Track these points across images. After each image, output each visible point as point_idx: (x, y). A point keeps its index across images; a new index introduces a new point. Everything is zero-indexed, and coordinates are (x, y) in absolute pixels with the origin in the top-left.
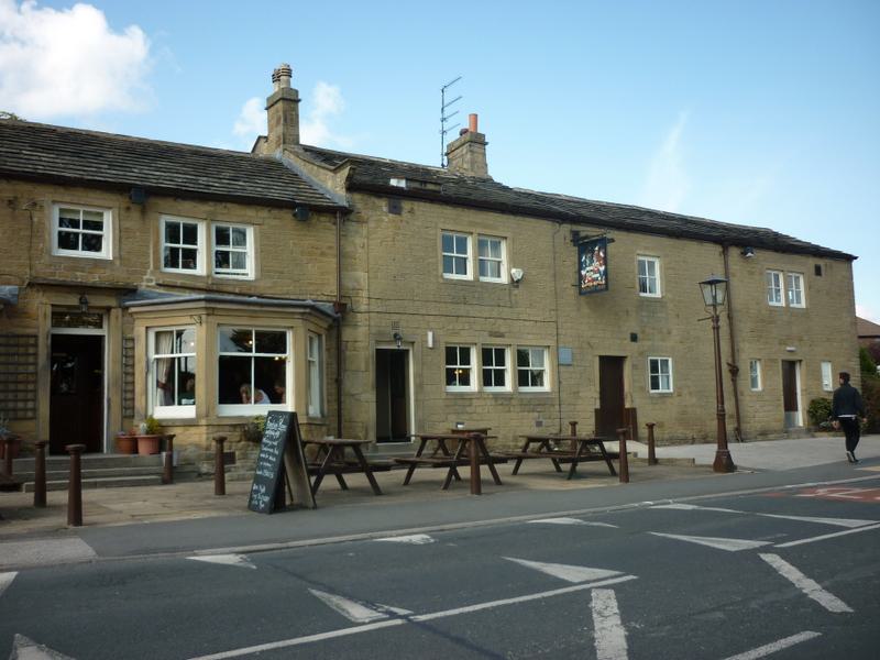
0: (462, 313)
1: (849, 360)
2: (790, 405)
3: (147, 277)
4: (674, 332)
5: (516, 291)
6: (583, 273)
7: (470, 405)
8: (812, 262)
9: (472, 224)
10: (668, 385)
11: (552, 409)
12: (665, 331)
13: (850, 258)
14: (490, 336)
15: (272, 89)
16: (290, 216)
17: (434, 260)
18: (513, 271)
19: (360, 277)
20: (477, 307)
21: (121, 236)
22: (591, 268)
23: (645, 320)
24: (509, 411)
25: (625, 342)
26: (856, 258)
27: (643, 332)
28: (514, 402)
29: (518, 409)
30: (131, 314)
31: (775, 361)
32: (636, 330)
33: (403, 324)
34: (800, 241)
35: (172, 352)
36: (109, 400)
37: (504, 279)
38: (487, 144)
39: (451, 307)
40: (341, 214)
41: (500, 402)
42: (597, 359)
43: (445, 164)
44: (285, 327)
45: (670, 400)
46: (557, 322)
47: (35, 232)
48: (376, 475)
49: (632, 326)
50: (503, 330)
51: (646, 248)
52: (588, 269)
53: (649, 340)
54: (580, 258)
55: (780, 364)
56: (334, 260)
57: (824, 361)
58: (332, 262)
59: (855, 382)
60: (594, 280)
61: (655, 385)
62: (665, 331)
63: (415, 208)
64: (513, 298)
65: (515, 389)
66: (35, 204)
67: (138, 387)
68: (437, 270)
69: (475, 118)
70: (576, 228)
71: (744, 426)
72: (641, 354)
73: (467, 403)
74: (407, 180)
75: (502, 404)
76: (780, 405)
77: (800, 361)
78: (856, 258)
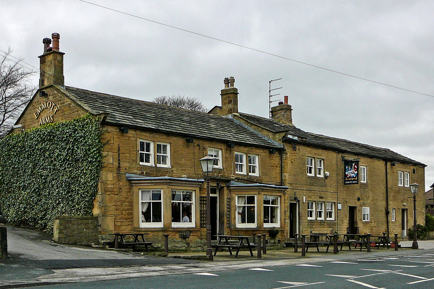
0: (312, 189)
1: (422, 209)
2: (403, 228)
3: (232, 175)
4: (370, 197)
5: (326, 181)
6: (347, 173)
8: (412, 167)
11: (335, 227)
12: (368, 196)
13: (424, 166)
14: (320, 198)
15: (223, 87)
16: (267, 152)
18: (326, 172)
21: (262, 165)
22: (351, 172)
23: (362, 192)
26: (426, 166)
27: (361, 197)
30: (132, 183)
32: (359, 196)
33: (297, 193)
34: (402, 156)
35: (245, 204)
37: (322, 176)
40: (281, 151)
43: (271, 116)
44: (192, 190)
46: (337, 193)
49: (358, 194)
50: (323, 196)
54: (345, 167)
55: (401, 210)
57: (340, 210)
58: (278, 170)
61: (364, 219)
62: (368, 196)
63: (300, 148)
65: (325, 219)
66: (204, 148)
67: (233, 217)
68: (306, 172)
69: (286, 98)
70: (343, 155)
74: (298, 137)
76: (53, 286)
77: (407, 209)
78: (426, 166)
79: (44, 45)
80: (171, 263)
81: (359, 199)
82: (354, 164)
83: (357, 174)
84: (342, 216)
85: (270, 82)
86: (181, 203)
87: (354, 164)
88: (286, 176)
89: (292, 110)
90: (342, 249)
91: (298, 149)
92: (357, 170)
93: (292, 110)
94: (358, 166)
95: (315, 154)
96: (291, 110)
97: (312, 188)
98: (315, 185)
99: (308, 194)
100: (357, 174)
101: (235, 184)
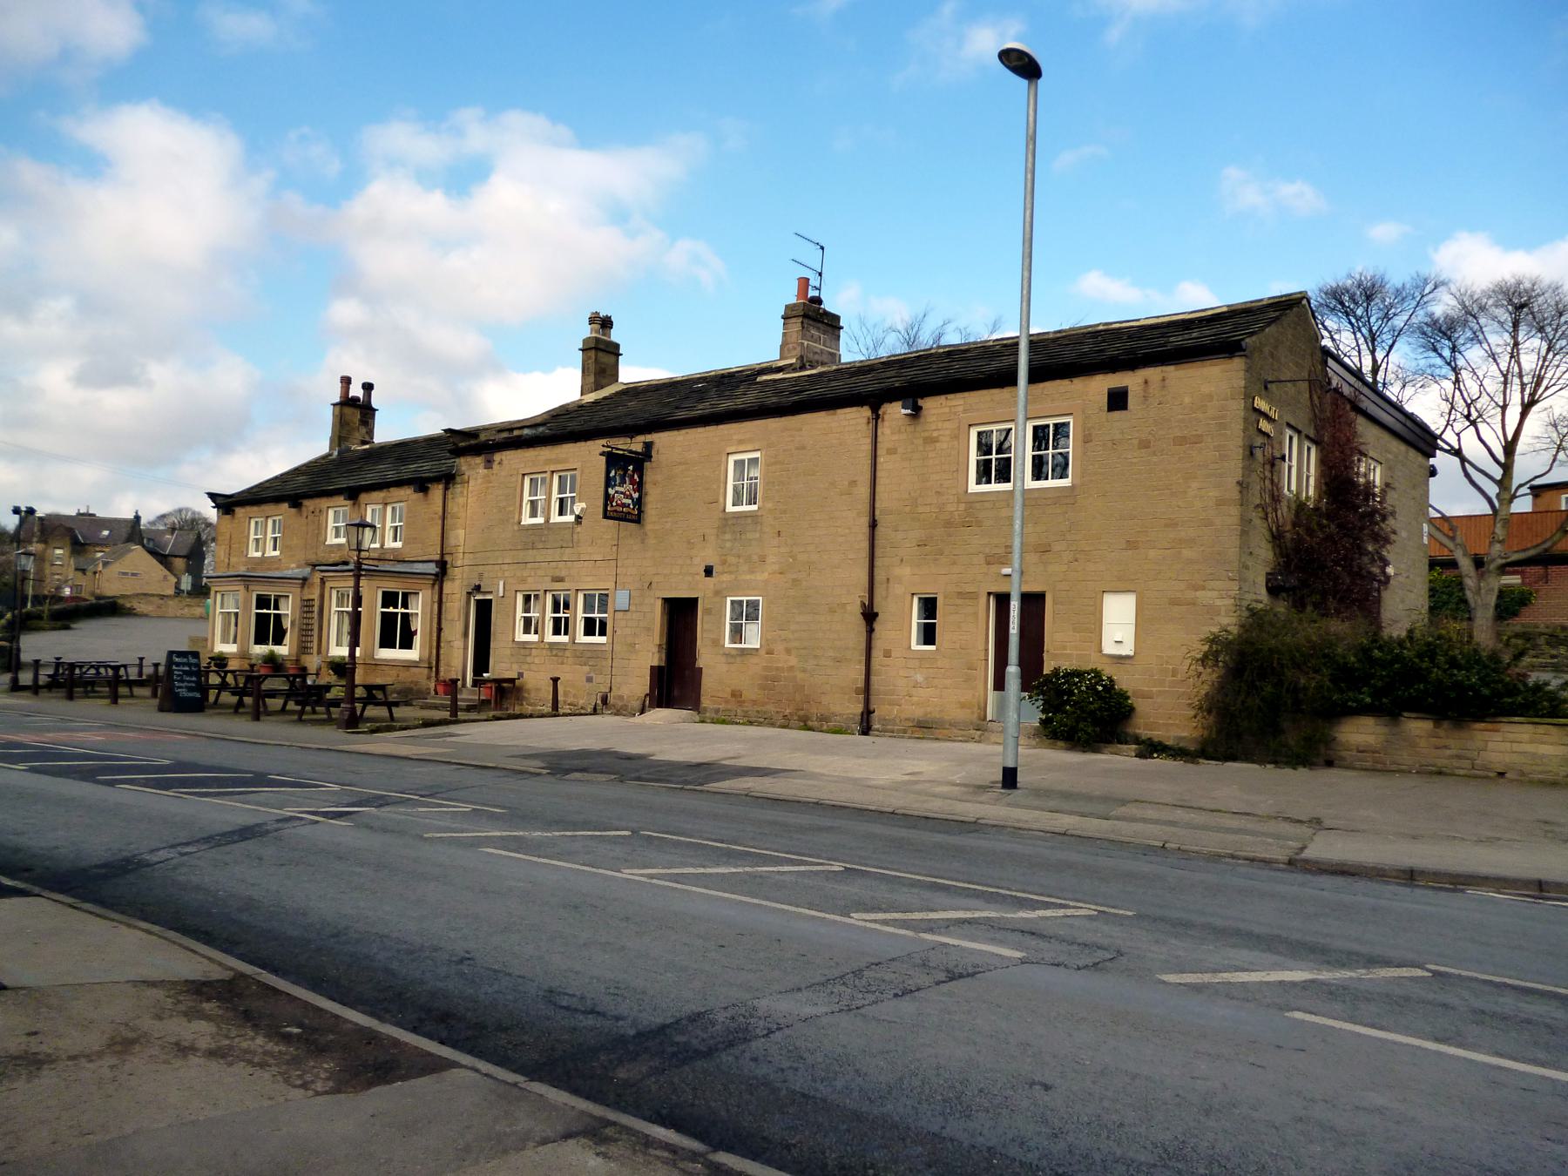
4: (771, 559)
5: (579, 529)
6: (611, 491)
7: (530, 655)
9: (549, 461)
10: (753, 636)
17: (511, 509)
19: (459, 536)
20: (544, 552)
23: (728, 545)
24: (562, 663)
25: (698, 577)
27: (724, 563)
28: (568, 654)
29: (570, 660)
31: (973, 596)
33: (486, 575)
36: (466, 634)
38: (842, 328)
39: (521, 553)
41: (554, 652)
42: (659, 603)
45: (754, 660)
47: (320, 530)
48: (394, 710)
50: (563, 574)
51: (741, 442)
52: (617, 488)
53: (731, 573)
54: (608, 472)
56: (1558, 457)
59: (161, 669)
60: (624, 505)
63: (504, 458)
64: (575, 536)
71: (881, 710)
72: (717, 593)
73: (527, 652)
75: (556, 656)
79: (340, 384)
80: (824, 855)
81: (709, 572)
82: (631, 468)
83: (640, 499)
84: (628, 631)
85: (822, 248)
86: (233, 615)
87: (631, 468)
88: (458, 536)
89: (621, 355)
90: (288, 708)
91: (499, 463)
92: (640, 487)
93: (621, 355)
94: (641, 477)
95: (549, 461)
96: (618, 355)
97: (530, 555)
98: (540, 546)
99: (519, 574)
100: (640, 499)
101: (1558, 535)
